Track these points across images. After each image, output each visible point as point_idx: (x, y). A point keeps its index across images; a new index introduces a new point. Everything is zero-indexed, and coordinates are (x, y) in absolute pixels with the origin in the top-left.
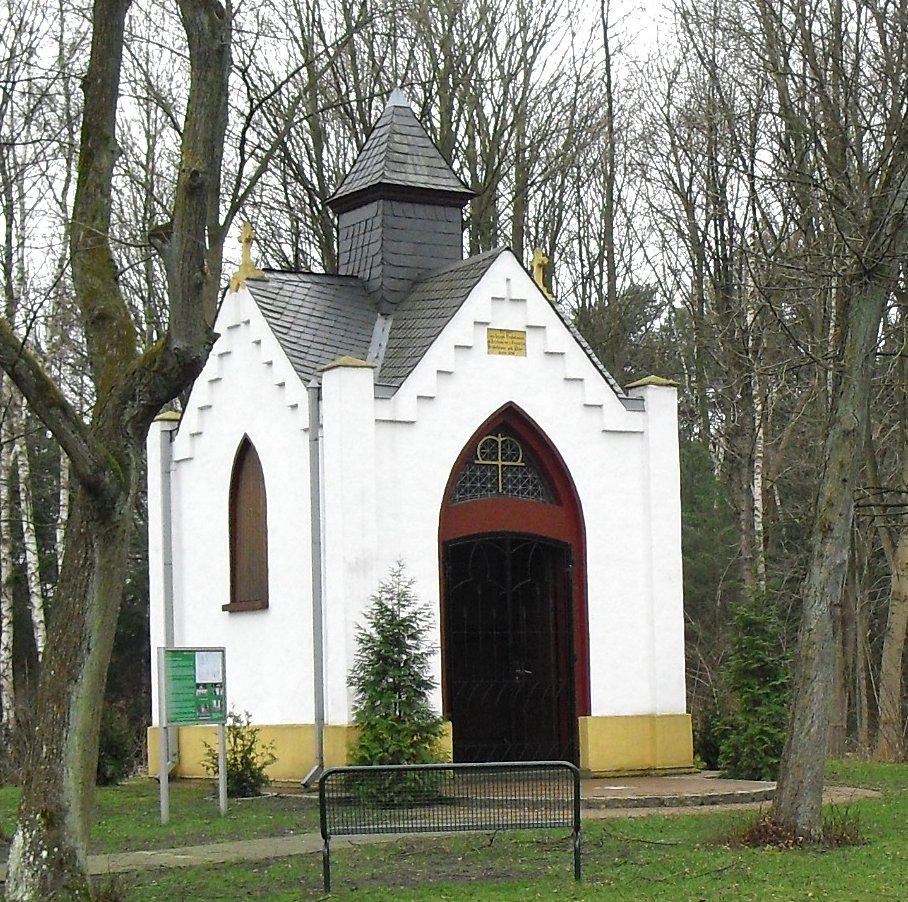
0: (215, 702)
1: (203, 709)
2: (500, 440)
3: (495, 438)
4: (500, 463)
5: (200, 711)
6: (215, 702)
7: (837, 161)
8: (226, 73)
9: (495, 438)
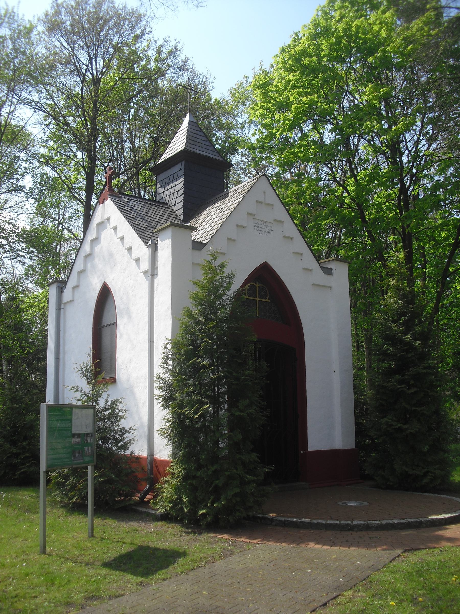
0: (86, 448)
1: (77, 455)
2: (257, 286)
3: (254, 284)
4: (257, 299)
5: (74, 456)
6: (86, 448)
7: (451, 403)
8: (182, 384)
9: (254, 284)
